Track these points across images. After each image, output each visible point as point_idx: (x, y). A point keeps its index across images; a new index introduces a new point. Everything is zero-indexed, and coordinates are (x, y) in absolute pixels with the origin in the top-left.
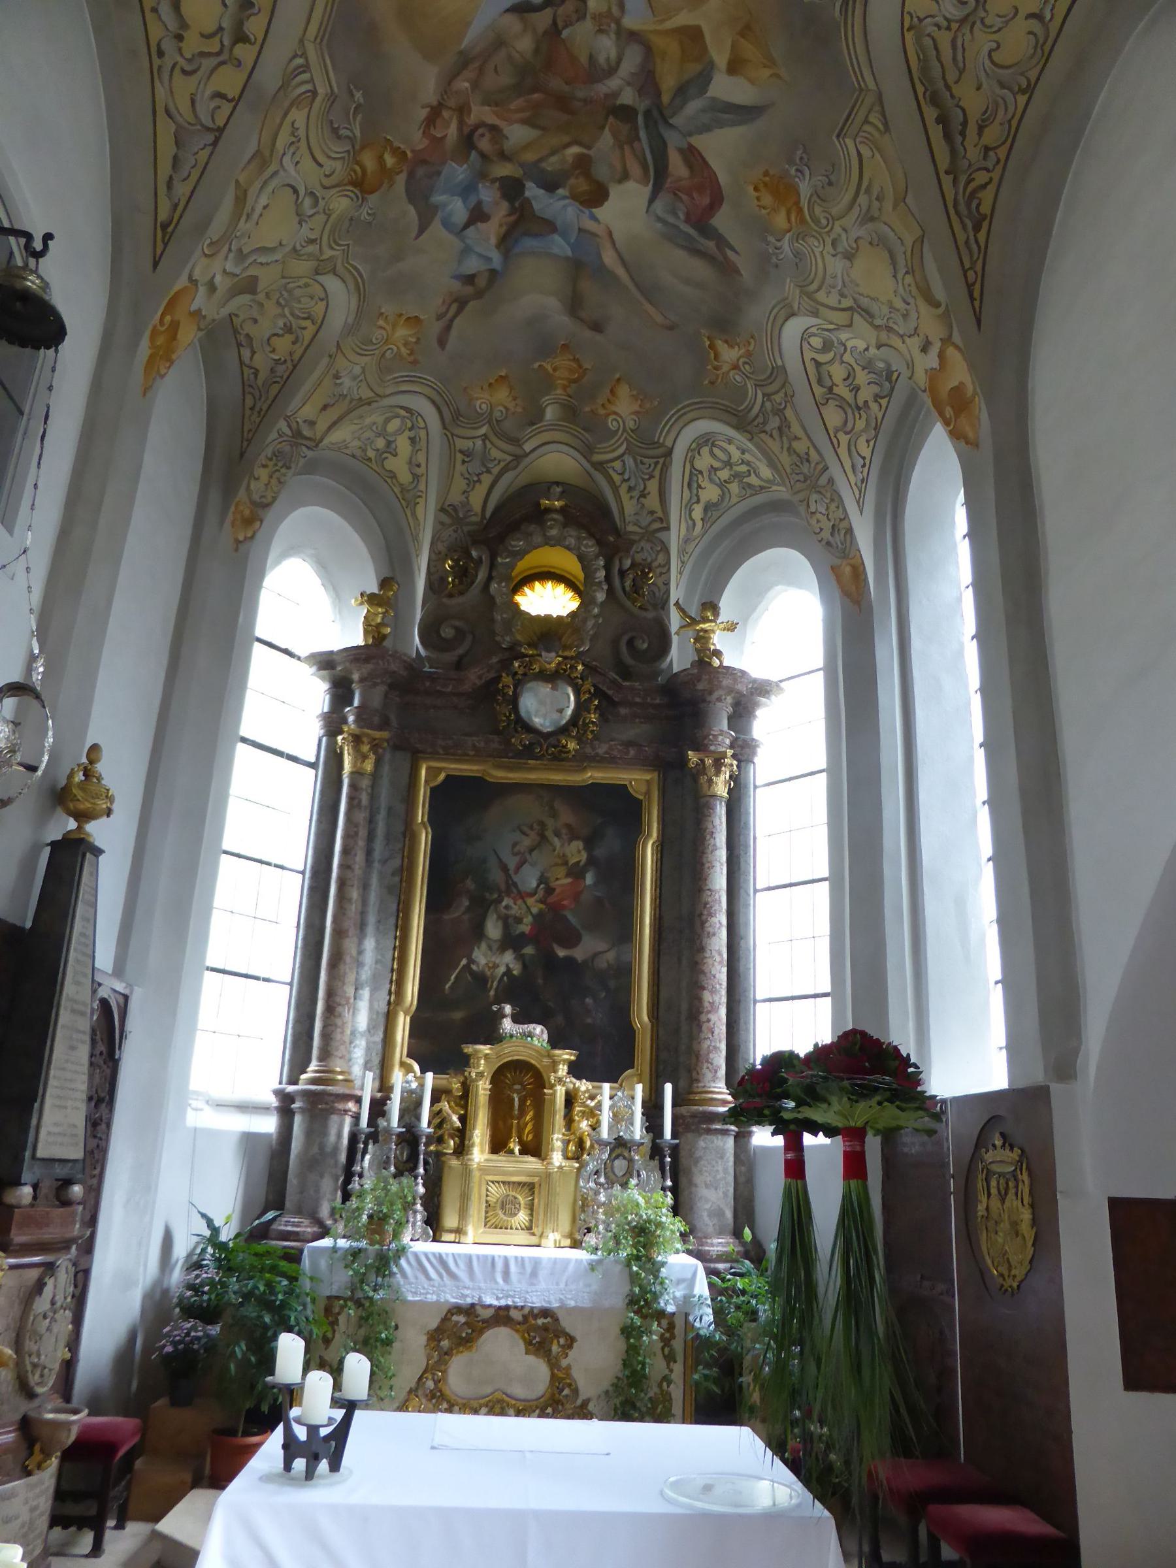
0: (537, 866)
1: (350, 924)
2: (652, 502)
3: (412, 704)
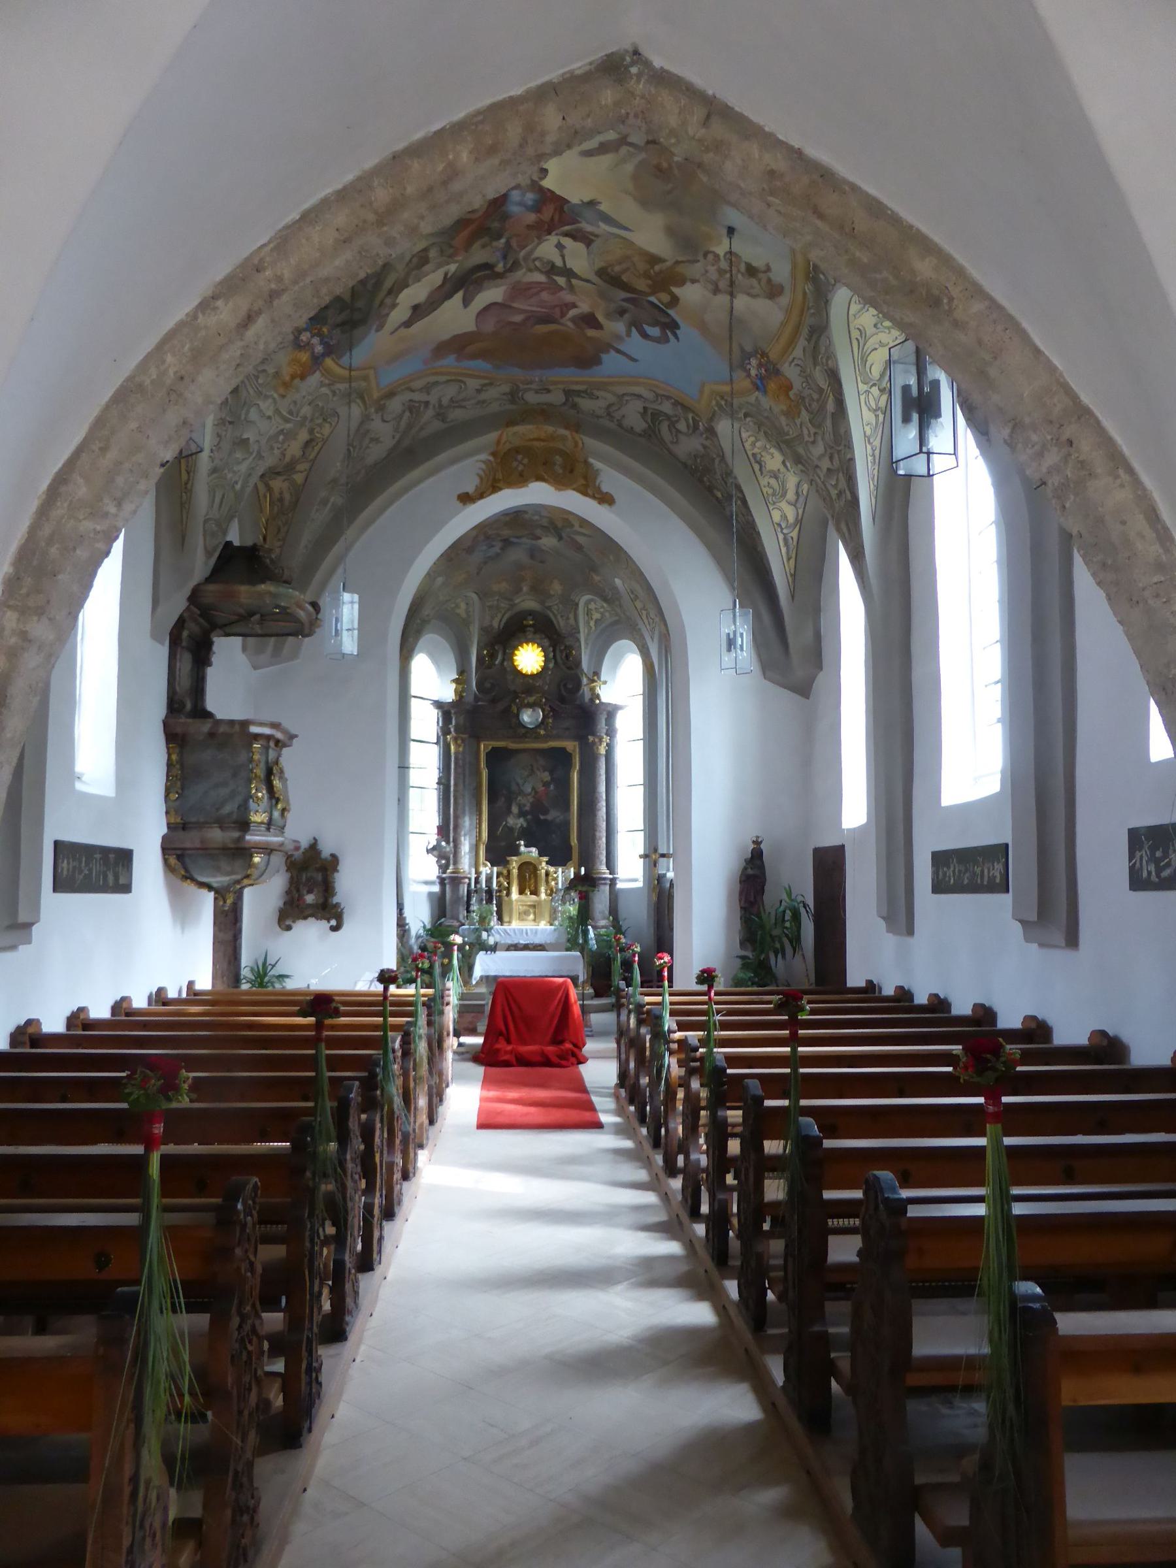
0: (530, 783)
1: (459, 812)
2: (572, 621)
3: (476, 720)
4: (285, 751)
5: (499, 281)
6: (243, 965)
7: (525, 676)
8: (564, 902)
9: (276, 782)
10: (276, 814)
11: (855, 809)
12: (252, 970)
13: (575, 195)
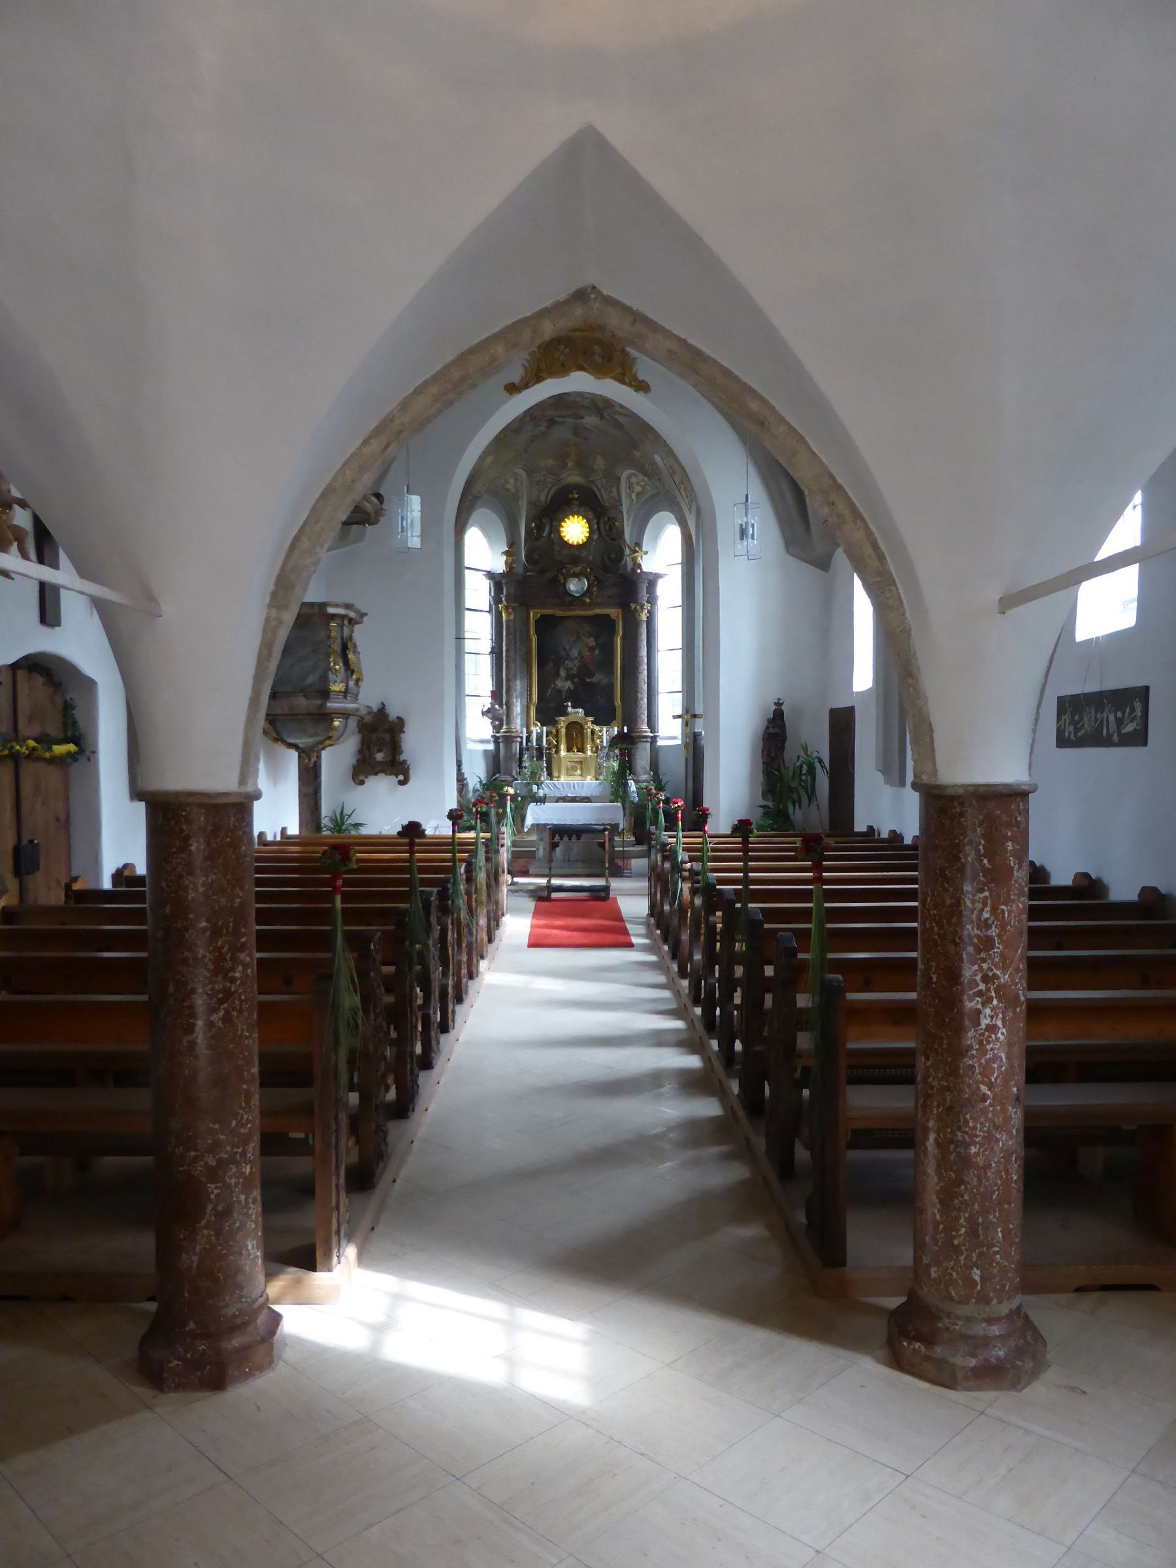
0: (577, 649)
2: (614, 494)
3: (527, 591)
4: (357, 627)
6: (323, 815)
7: (572, 546)
8: (608, 757)
10: (351, 683)
11: (863, 677)
12: (331, 820)
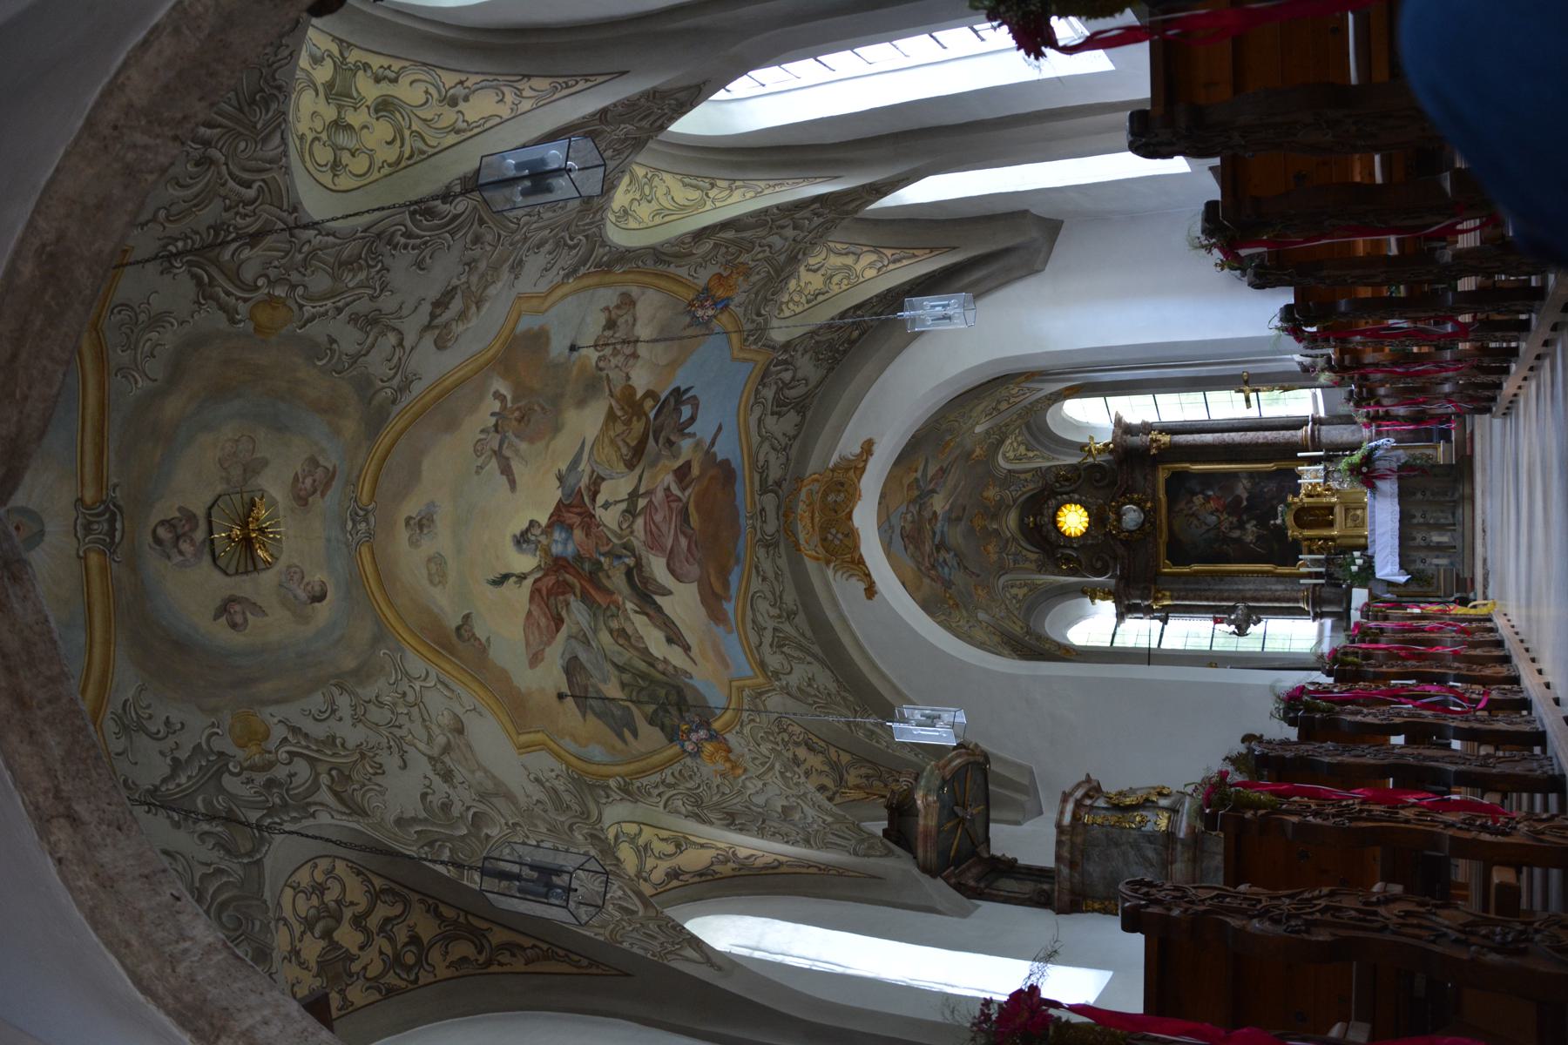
0: (1206, 512)
5: (644, 561)
9: (1128, 801)
13: (554, 495)
